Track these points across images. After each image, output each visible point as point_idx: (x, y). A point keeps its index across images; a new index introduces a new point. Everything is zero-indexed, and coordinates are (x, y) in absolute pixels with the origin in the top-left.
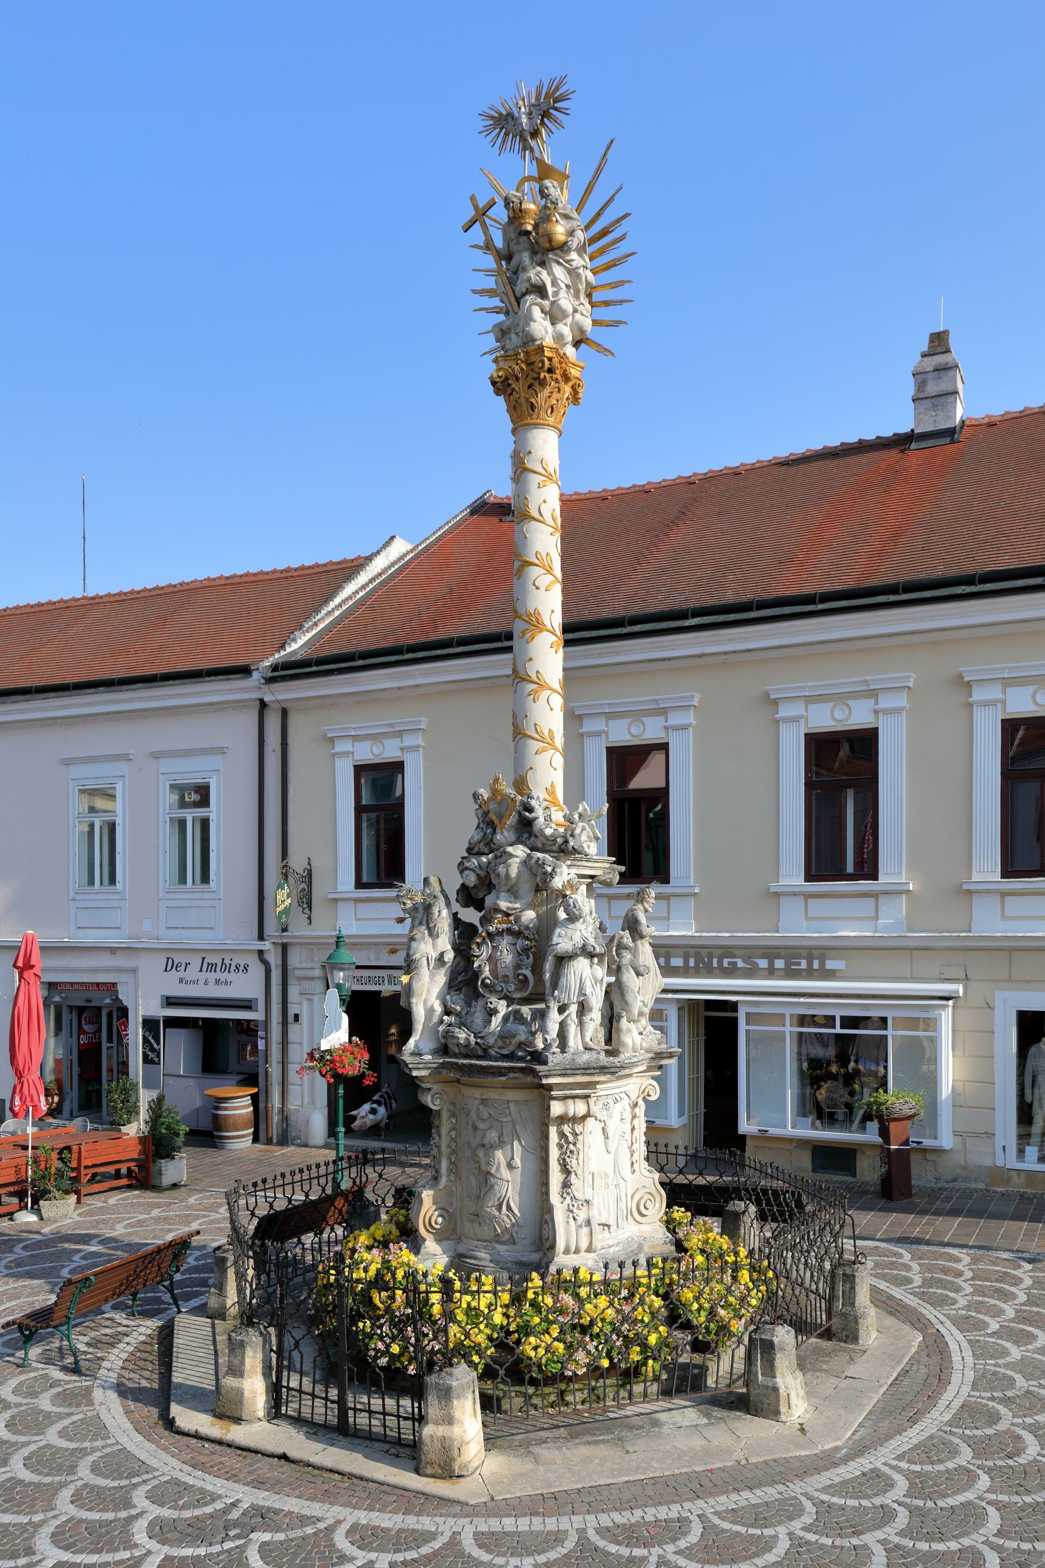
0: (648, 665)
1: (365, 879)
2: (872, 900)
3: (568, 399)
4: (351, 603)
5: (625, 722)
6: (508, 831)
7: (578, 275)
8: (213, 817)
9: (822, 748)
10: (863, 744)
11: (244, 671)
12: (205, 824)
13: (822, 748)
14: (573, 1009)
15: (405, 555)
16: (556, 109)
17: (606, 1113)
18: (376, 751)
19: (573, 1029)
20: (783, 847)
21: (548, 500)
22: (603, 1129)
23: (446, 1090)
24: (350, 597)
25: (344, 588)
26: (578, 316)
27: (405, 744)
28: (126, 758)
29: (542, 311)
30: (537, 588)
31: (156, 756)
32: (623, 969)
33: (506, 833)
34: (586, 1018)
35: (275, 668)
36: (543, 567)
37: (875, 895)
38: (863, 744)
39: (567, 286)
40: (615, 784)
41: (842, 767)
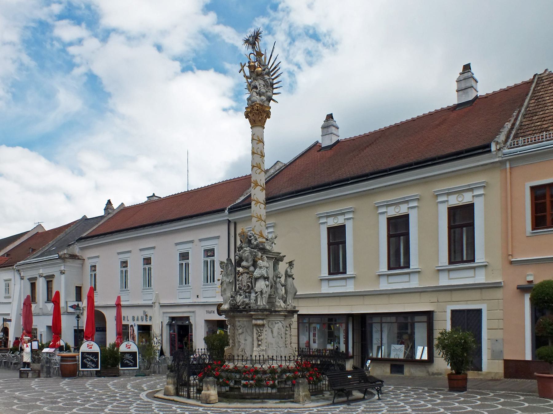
0: (389, 187)
1: (392, 266)
2: (408, 276)
5: (332, 218)
8: (152, 267)
9: (453, 211)
10: (469, 208)
11: (223, 210)
12: (95, 275)
13: (453, 211)
18: (460, 199)
19: (259, 299)
20: (18, 294)
27: (346, 217)
28: (192, 242)
31: (201, 240)
35: (229, 209)
37: (474, 268)
38: (469, 208)
40: (452, 221)
41: (398, 228)
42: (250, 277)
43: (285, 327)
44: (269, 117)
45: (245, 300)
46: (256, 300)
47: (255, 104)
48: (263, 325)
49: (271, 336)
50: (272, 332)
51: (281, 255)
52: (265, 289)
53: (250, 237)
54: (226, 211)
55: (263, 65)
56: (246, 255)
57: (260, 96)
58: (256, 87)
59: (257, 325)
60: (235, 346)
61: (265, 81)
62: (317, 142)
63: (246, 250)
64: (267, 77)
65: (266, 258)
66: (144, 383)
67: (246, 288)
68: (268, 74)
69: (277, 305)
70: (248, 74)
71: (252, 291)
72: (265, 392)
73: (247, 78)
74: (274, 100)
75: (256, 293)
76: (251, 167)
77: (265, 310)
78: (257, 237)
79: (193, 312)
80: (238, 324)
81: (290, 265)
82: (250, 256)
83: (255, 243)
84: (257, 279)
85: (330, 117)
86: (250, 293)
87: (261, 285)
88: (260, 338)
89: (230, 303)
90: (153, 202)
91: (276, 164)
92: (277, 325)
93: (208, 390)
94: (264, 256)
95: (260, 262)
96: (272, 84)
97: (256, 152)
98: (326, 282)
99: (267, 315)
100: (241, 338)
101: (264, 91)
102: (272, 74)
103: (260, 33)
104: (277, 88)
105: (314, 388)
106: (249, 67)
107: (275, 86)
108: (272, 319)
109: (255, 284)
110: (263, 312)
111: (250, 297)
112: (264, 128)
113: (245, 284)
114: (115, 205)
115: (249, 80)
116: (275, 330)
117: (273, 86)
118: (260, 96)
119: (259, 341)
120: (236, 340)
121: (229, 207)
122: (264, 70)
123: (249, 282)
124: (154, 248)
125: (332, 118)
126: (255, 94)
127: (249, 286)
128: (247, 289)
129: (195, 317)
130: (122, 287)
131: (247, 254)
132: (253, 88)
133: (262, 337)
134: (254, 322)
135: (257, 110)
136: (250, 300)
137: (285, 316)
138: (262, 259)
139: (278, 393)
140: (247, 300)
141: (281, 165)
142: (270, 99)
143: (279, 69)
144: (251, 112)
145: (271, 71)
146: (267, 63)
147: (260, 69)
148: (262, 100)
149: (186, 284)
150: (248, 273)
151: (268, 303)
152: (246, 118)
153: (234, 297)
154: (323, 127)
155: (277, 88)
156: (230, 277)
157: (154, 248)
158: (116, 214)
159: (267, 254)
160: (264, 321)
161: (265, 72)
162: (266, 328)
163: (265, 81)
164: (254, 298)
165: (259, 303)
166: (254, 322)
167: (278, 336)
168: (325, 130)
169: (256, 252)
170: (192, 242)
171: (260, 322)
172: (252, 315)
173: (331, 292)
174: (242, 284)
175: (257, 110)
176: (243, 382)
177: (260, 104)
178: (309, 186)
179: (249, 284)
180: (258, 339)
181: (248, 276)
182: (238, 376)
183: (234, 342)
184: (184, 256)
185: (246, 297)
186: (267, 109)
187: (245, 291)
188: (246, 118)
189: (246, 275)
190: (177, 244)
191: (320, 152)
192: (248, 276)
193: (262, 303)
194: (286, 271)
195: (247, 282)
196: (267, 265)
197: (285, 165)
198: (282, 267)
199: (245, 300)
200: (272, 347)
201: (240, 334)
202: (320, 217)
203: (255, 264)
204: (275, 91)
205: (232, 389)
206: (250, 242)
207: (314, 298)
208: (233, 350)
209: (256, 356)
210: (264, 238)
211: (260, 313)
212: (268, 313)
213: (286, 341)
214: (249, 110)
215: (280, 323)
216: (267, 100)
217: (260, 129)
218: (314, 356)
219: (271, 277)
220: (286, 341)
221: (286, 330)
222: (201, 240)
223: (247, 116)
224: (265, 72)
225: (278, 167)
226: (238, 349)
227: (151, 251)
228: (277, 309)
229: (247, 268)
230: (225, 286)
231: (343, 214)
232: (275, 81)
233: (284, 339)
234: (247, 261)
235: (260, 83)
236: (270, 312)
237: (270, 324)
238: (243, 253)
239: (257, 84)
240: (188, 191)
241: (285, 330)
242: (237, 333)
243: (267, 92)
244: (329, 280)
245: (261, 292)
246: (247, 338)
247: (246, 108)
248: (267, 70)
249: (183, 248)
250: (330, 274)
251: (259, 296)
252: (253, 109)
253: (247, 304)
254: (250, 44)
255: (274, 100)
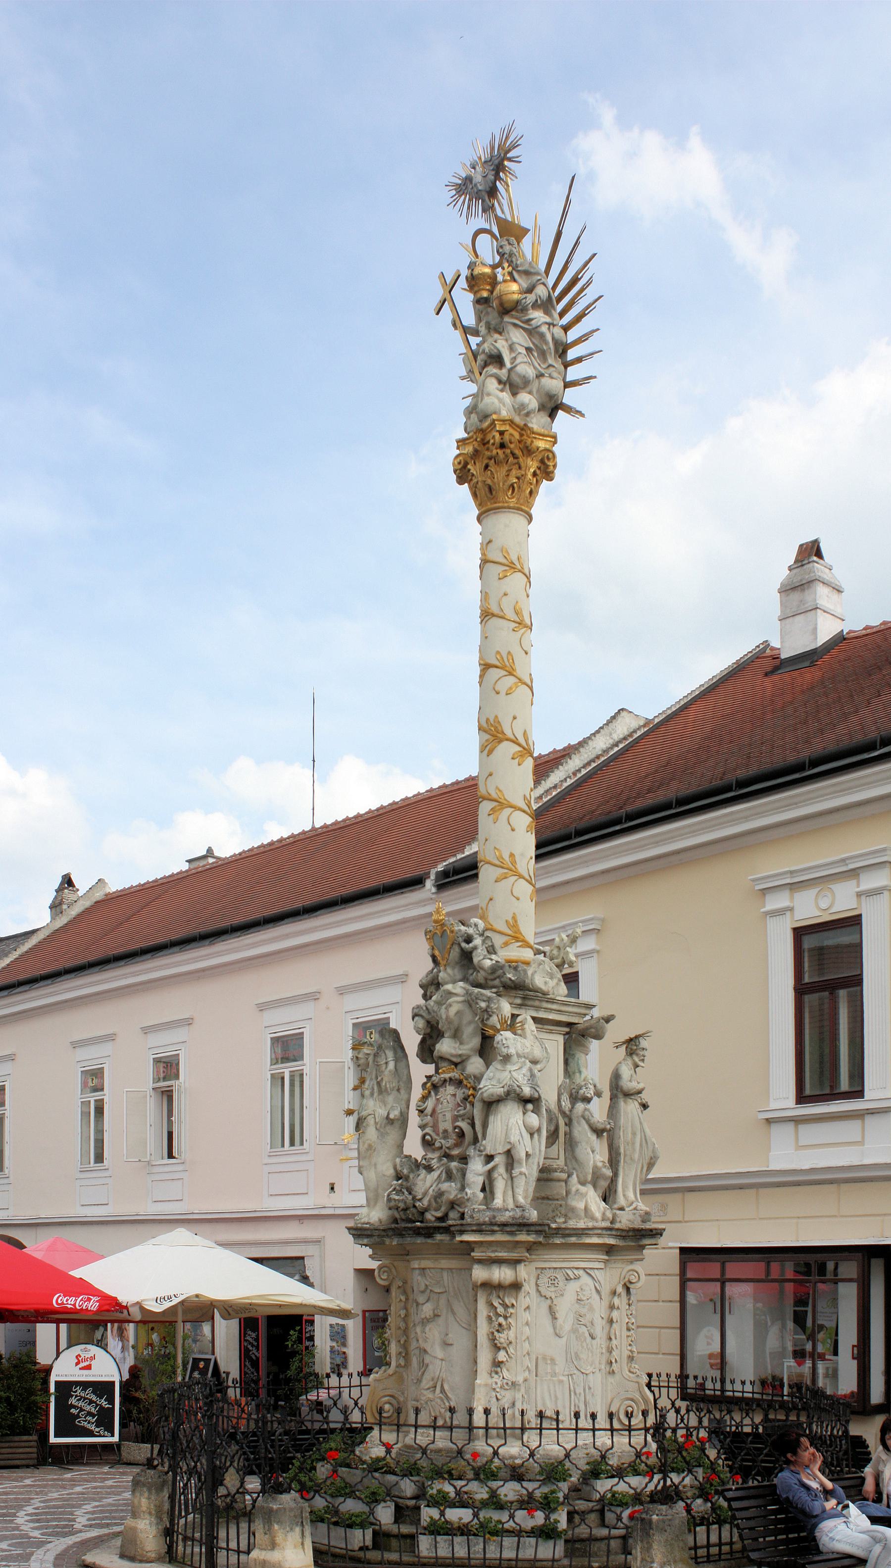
3: (535, 474)
4: (554, 793)
6: (453, 968)
7: (542, 336)
11: (417, 882)
14: (499, 1160)
15: (635, 731)
16: (510, 160)
17: (553, 1289)
19: (500, 1185)
21: (508, 592)
22: (550, 1307)
23: (396, 1263)
24: (555, 787)
25: (548, 776)
26: (545, 381)
28: (314, 997)
29: (500, 382)
30: (498, 693)
31: (342, 991)
32: (575, 1122)
33: (449, 970)
34: (515, 1172)
35: (445, 874)
36: (503, 668)
39: (528, 349)
42: (465, 1099)
43: (606, 1292)
44: (549, 476)
45: (445, 1186)
46: (487, 1188)
47: (493, 422)
48: (516, 1286)
49: (551, 1330)
50: (552, 1313)
51: (596, 1013)
52: (524, 1145)
53: (469, 939)
54: (429, 884)
55: (527, 273)
56: (453, 1011)
57: (514, 394)
58: (497, 359)
59: (487, 1286)
60: (408, 1364)
61: (532, 332)
62: (766, 644)
63: (450, 994)
64: (538, 316)
65: (531, 1026)
66: (84, 1498)
67: (451, 1142)
68: (546, 305)
69: (573, 1210)
70: (469, 318)
71: (471, 1152)
72: (509, 1554)
73: (466, 331)
74: (568, 409)
75: (490, 1158)
76: (477, 670)
77: (523, 1225)
78: (498, 940)
79: (318, 1241)
80: (418, 1281)
81: (631, 1053)
82: (468, 1016)
83: (488, 963)
84: (490, 1105)
85: (811, 551)
86: (464, 1159)
87: (510, 1126)
88: (502, 1338)
89: (389, 1200)
90: (206, 872)
91: (614, 718)
92: (573, 1286)
93: (273, 1546)
94: (526, 1016)
95: (506, 1040)
96: (562, 349)
97: (495, 609)
98: (790, 1127)
99: (531, 1247)
100: (431, 1337)
101: (531, 372)
102: (560, 307)
103: (514, 146)
104: (579, 360)
105: (714, 1539)
106: (473, 282)
107: (572, 354)
108: (553, 1260)
109: (485, 1126)
110: (511, 1233)
111: (464, 1175)
112: (530, 519)
113: (446, 1124)
114: (83, 885)
115: (474, 341)
116: (565, 1306)
117: (564, 352)
118: (514, 394)
119: (497, 1348)
120: (414, 1344)
121: (440, 868)
122: (530, 290)
123: (462, 1117)
124: (188, 1022)
125: (819, 554)
126: (492, 385)
127: (462, 1135)
128: (457, 1145)
129: (322, 1258)
130: (84, 1153)
131: (455, 1006)
132: (486, 365)
133: (512, 1334)
134: (479, 1273)
135: (502, 446)
136: (463, 1188)
137: (609, 1250)
138: (512, 1024)
139: (566, 1562)
140: (451, 1189)
141: (634, 724)
142: (553, 407)
143: (589, 283)
144: (476, 454)
145: (559, 299)
146: (542, 266)
147: (514, 287)
148: (522, 406)
149: (292, 1144)
150: (459, 1083)
151: (541, 1198)
152: (461, 480)
153: (407, 1178)
154: (789, 589)
155: (579, 360)
156: (390, 1099)
157: (188, 1022)
158: (79, 915)
159: (537, 1008)
160: (521, 1268)
161: (531, 298)
162: (527, 1298)
163: (532, 332)
164: (480, 1180)
165: (498, 1202)
166: (479, 1273)
167: (574, 1331)
168: (795, 596)
169: (489, 1000)
170: (314, 997)
171: (502, 1274)
172: (470, 1247)
173: (806, 1167)
174: (435, 1127)
175: (502, 446)
176: (429, 1514)
177: (511, 422)
178: (730, 778)
179: (464, 1125)
180: (493, 1340)
181: (460, 1094)
182: (408, 1487)
183: (405, 1354)
184: (288, 1048)
185: (450, 1176)
186: (541, 444)
187: (447, 1156)
188: (461, 480)
189: (450, 1089)
190: (262, 1007)
191: (775, 678)
192: (460, 1094)
193: (514, 1196)
194: (616, 1076)
195: (455, 1118)
196: (537, 1053)
197: (648, 722)
198: (597, 1062)
199: (445, 1186)
200: (554, 1374)
201: (425, 1322)
202: (764, 891)
203: (486, 1047)
204: (573, 373)
205: (381, 1539)
206: (467, 957)
207: (741, 1187)
208: (401, 1380)
209: (487, 1412)
210: (527, 945)
211: (499, 1237)
212: (531, 1238)
213: (610, 1351)
214: (469, 449)
215: (585, 1279)
216: (542, 408)
217: (515, 520)
218: (745, 1404)
219: (550, 1096)
220: (610, 1351)
221: (612, 1307)
222: (342, 991)
223: (463, 475)
224: (531, 298)
225: (621, 729)
226: (419, 1381)
227: (180, 1035)
228: (572, 1224)
229: (458, 1063)
230: (371, 1133)
231: (854, 874)
232: (572, 335)
233: (601, 1342)
234: (456, 1035)
235: (513, 342)
236: (542, 1234)
237: (544, 1281)
238: (439, 1003)
239: (502, 345)
240: (314, 829)
241: (605, 1303)
242: (415, 1318)
243: (540, 376)
244: (798, 1121)
245: (508, 1153)
246: (451, 1338)
247: (461, 443)
248: (541, 291)
249: (283, 1021)
250: (802, 1098)
251: (501, 1170)
252: (484, 443)
253: (452, 1205)
254: (477, 195)
255: (568, 409)
